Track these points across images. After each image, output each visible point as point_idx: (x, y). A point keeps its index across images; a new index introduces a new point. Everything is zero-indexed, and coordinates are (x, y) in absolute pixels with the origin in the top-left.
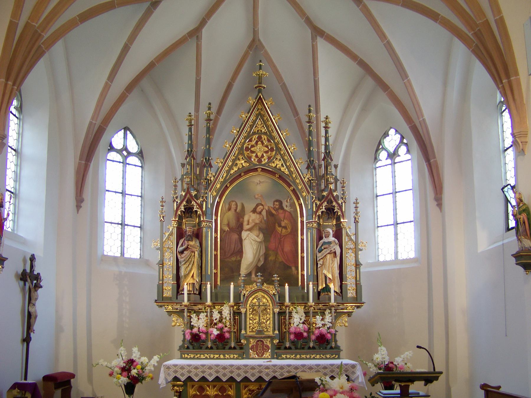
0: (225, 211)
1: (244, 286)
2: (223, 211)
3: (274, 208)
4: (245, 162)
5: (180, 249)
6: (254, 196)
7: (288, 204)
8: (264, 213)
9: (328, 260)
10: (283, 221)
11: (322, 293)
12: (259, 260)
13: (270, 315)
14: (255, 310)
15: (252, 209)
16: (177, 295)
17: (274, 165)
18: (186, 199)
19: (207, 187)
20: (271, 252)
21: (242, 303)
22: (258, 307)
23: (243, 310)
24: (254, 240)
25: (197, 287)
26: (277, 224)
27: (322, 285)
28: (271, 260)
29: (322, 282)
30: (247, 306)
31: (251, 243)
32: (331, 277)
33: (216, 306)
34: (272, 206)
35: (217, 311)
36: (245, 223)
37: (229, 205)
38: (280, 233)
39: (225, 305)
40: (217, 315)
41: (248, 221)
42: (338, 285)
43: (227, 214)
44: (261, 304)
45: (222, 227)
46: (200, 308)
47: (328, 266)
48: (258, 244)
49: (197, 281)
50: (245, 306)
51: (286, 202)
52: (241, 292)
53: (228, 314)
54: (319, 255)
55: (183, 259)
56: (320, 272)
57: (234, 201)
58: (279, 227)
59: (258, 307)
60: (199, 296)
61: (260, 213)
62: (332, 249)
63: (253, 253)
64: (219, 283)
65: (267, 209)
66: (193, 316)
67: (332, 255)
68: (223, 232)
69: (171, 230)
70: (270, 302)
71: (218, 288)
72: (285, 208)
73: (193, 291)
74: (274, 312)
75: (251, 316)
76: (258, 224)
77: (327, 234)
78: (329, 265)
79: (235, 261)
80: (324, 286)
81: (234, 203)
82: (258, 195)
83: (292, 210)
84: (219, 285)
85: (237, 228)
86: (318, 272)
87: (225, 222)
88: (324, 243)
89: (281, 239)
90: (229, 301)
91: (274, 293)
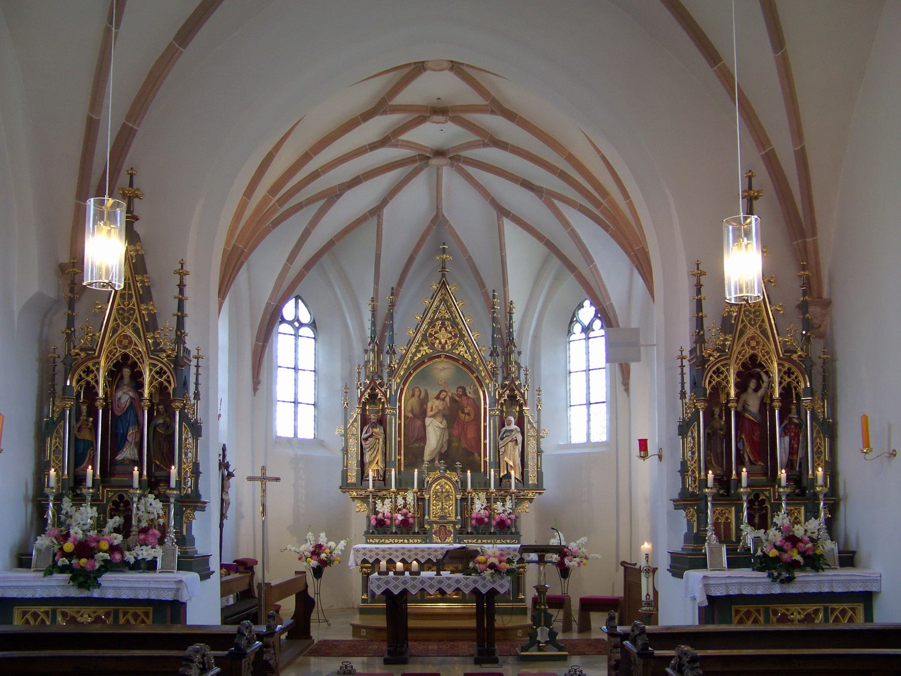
7: (471, 391)
8: (447, 399)
23: (426, 497)
26: (460, 411)
27: (504, 472)
29: (504, 469)
32: (512, 464)
34: (456, 393)
36: (429, 410)
41: (432, 408)
44: (444, 490)
61: (444, 400)
64: (402, 469)
70: (453, 488)
71: (402, 475)
72: (469, 395)
83: (475, 396)
87: (409, 408)
88: (506, 431)
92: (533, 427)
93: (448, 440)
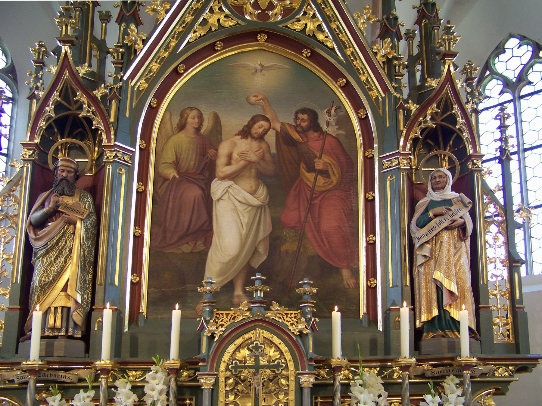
0: (170, 132)
1: (211, 313)
2: (163, 131)
3: (295, 127)
4: (226, 16)
5: (37, 215)
6: (248, 99)
7: (332, 120)
8: (271, 137)
9: (445, 245)
10: (320, 158)
11: (428, 332)
12: (255, 251)
13: (286, 394)
14: (243, 381)
15: (241, 128)
16: (18, 342)
17: (298, 27)
18: (59, 87)
19: (125, 65)
20: (286, 232)
21: (204, 360)
22: (253, 370)
23: (206, 382)
24: (243, 201)
25: (77, 317)
26: (302, 165)
27: (429, 311)
28: (287, 251)
29: (429, 303)
30: (218, 370)
31: (236, 210)
32: (454, 289)
33: (131, 370)
34: (292, 123)
35: (129, 386)
36: (221, 160)
37: (182, 116)
38: (311, 186)
39: (153, 367)
40: (128, 398)
41: (230, 157)
42: (473, 310)
43: (175, 138)
44: (263, 362)
45: (160, 170)
46: (83, 376)
47: (445, 260)
48: (254, 212)
49: (76, 302)
50: (211, 369)
51: (326, 115)
52: (202, 328)
53: (160, 393)
54: (421, 235)
55: (40, 244)
56: (423, 277)
57: (196, 109)
58: (308, 172)
59: (253, 370)
60: (81, 345)
61: (261, 138)
62: (456, 217)
63: (241, 234)
64: (144, 309)
65: (279, 130)
66: (54, 401)
67: (456, 232)
68: (161, 180)
69: (18, 170)
70: (288, 356)
71: (141, 323)
72: (325, 128)
73: (64, 329)
74: (300, 384)
75: (231, 398)
76: (254, 162)
77: (441, 180)
78: (449, 259)
79: (191, 253)
80: (435, 312)
81: (194, 113)
82: (255, 96)
83: (341, 132)
84: (145, 313)
85: (199, 171)
86: (416, 280)
87: (169, 156)
88: (433, 204)
89: (313, 199)
90: (166, 355)
91: (300, 332)
92: (494, 200)
93: (271, 233)
